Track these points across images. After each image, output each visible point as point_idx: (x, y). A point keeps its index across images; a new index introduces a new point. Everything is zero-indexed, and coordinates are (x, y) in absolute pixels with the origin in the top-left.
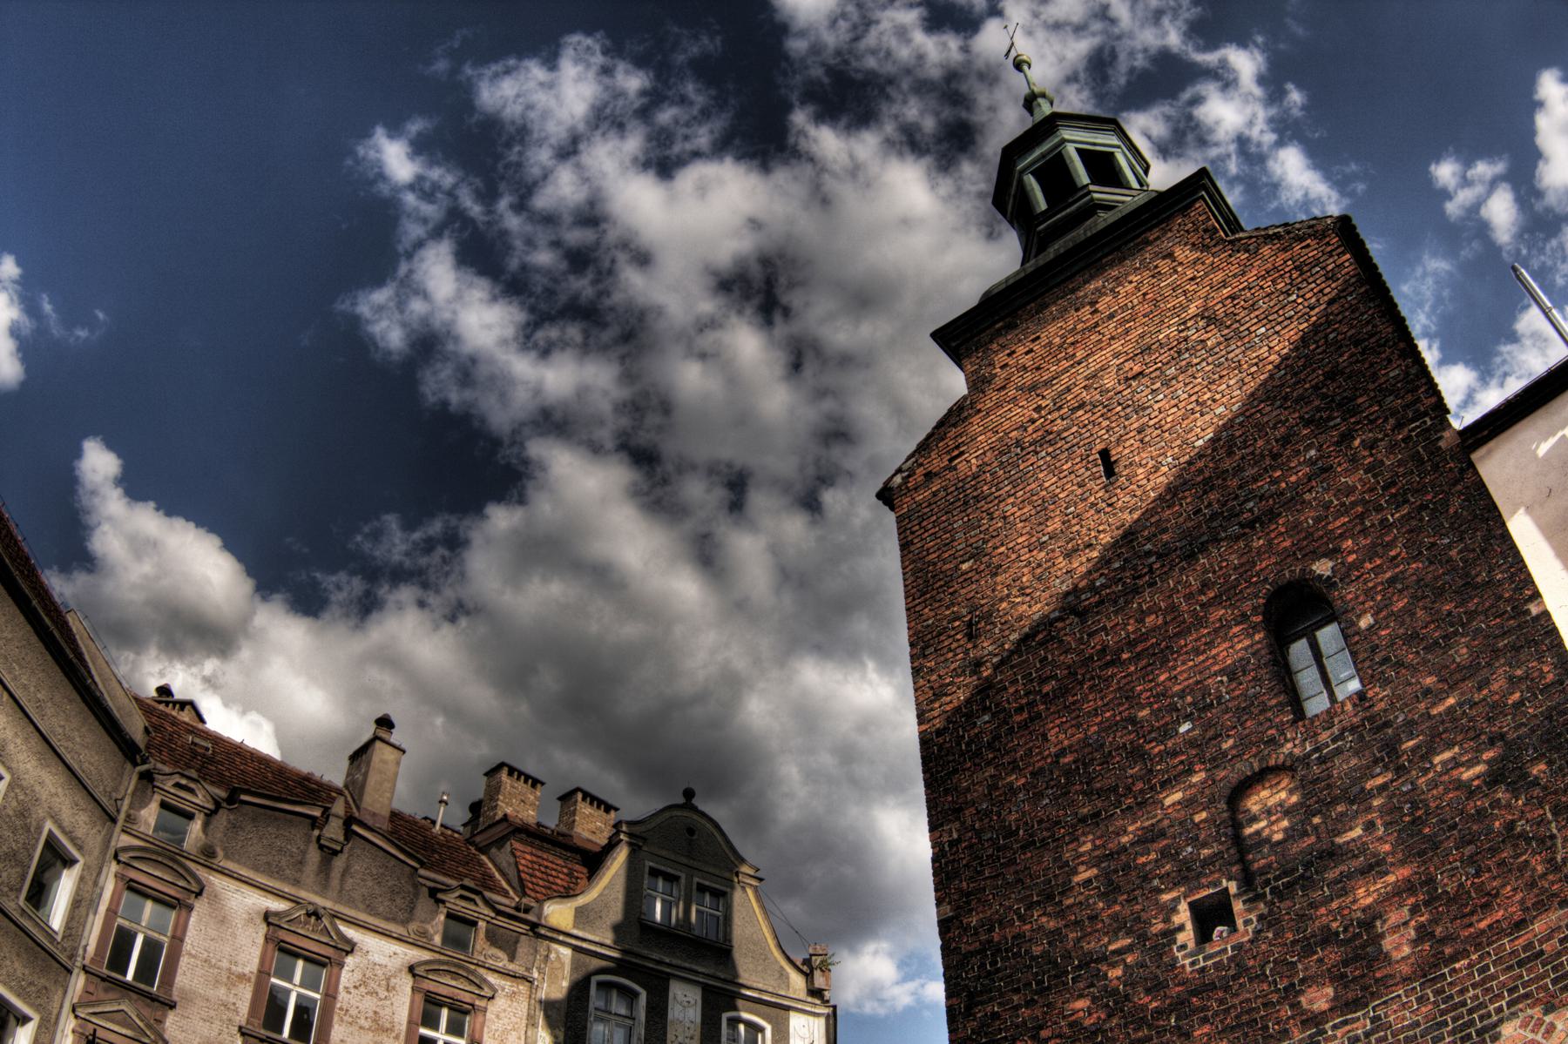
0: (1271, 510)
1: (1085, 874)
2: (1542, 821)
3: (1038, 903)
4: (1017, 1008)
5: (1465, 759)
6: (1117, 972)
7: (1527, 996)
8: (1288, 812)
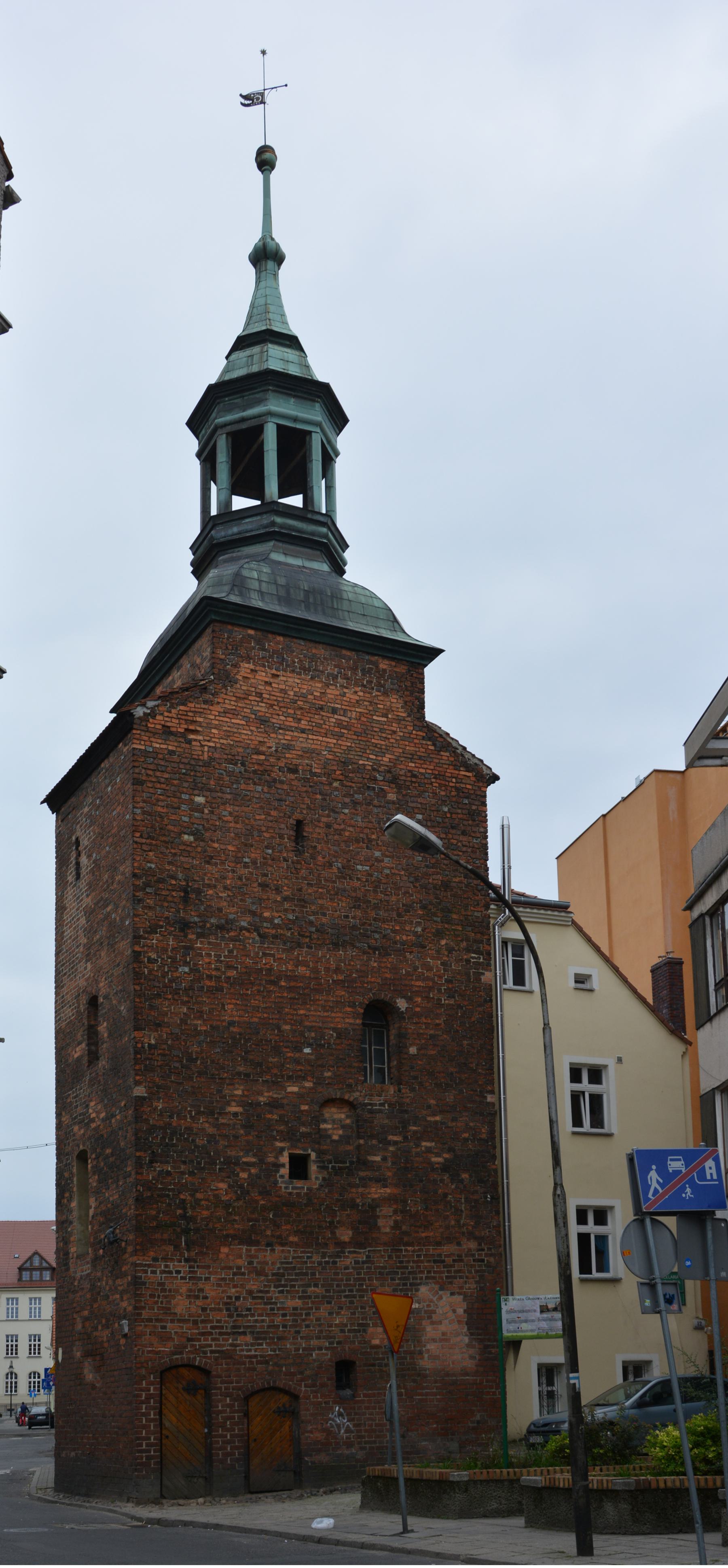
1: (234, 1109)
4: (183, 1173)
5: (436, 1151)
6: (243, 1175)
7: (434, 1278)
8: (343, 1127)
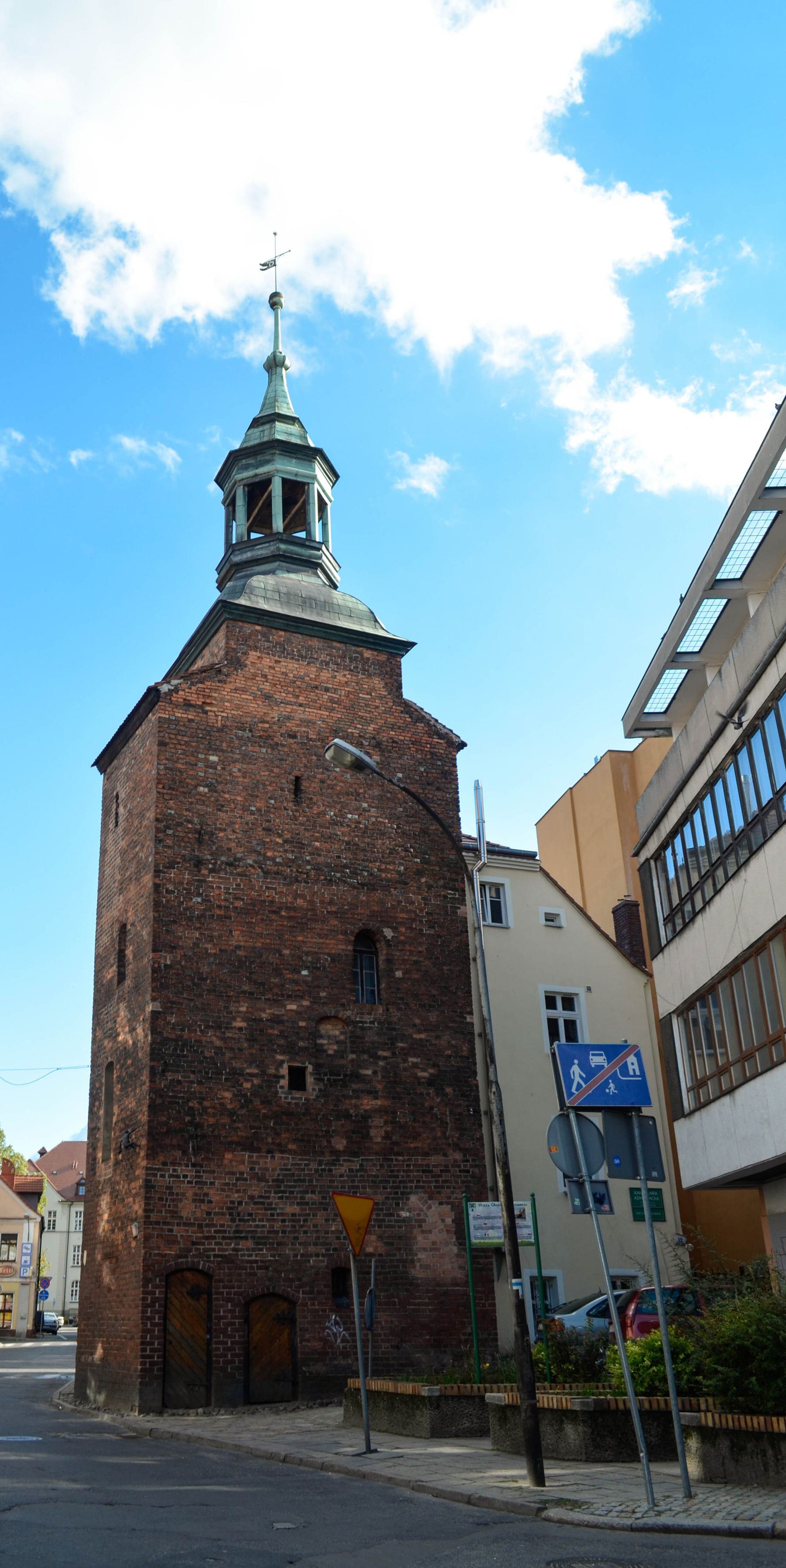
0: (373, 885)
1: (239, 1023)
2: (444, 1114)
3: (212, 1027)
4: (192, 1082)
6: (247, 1085)
7: (423, 1187)
